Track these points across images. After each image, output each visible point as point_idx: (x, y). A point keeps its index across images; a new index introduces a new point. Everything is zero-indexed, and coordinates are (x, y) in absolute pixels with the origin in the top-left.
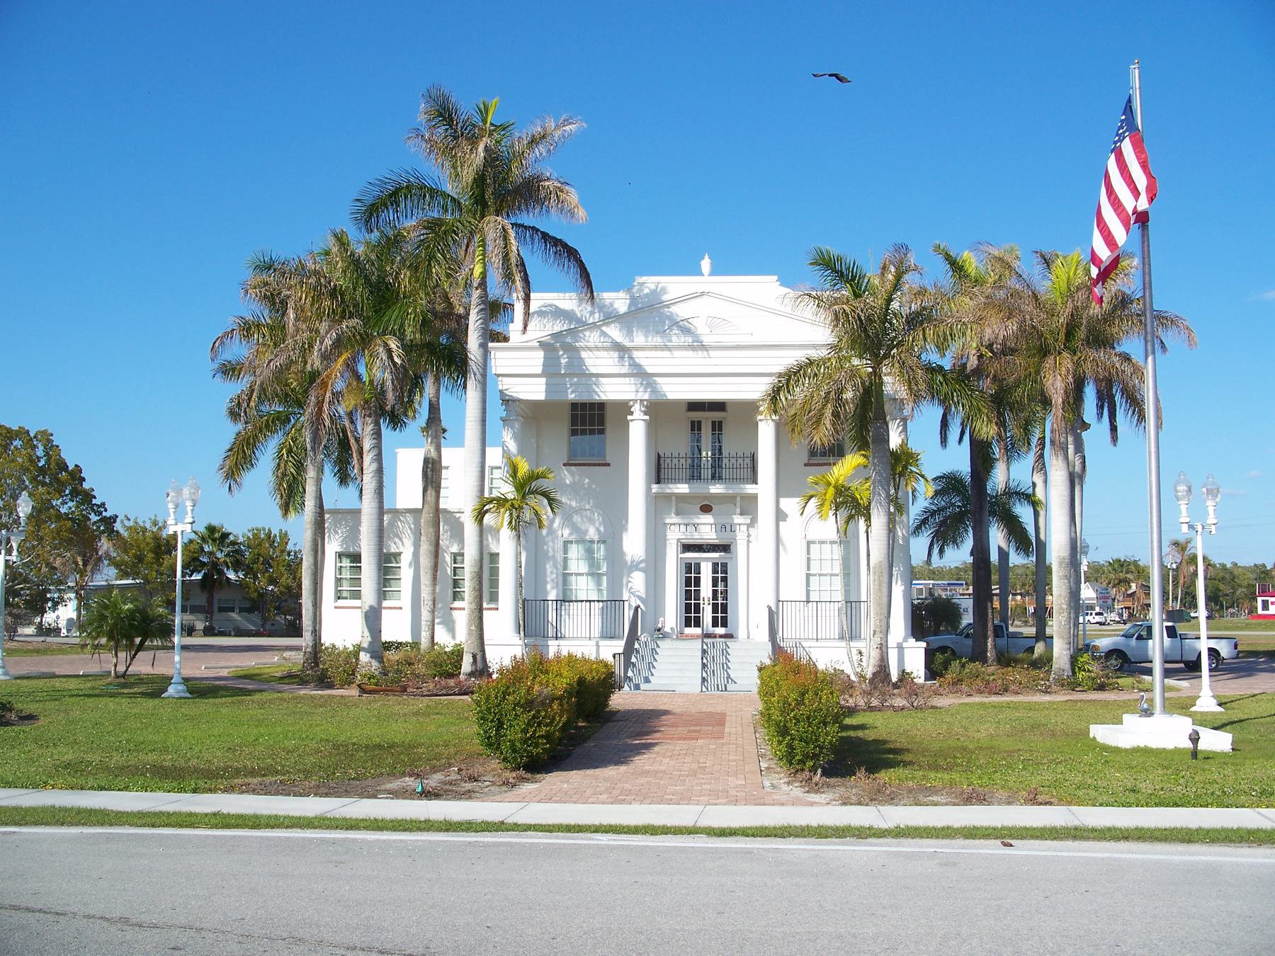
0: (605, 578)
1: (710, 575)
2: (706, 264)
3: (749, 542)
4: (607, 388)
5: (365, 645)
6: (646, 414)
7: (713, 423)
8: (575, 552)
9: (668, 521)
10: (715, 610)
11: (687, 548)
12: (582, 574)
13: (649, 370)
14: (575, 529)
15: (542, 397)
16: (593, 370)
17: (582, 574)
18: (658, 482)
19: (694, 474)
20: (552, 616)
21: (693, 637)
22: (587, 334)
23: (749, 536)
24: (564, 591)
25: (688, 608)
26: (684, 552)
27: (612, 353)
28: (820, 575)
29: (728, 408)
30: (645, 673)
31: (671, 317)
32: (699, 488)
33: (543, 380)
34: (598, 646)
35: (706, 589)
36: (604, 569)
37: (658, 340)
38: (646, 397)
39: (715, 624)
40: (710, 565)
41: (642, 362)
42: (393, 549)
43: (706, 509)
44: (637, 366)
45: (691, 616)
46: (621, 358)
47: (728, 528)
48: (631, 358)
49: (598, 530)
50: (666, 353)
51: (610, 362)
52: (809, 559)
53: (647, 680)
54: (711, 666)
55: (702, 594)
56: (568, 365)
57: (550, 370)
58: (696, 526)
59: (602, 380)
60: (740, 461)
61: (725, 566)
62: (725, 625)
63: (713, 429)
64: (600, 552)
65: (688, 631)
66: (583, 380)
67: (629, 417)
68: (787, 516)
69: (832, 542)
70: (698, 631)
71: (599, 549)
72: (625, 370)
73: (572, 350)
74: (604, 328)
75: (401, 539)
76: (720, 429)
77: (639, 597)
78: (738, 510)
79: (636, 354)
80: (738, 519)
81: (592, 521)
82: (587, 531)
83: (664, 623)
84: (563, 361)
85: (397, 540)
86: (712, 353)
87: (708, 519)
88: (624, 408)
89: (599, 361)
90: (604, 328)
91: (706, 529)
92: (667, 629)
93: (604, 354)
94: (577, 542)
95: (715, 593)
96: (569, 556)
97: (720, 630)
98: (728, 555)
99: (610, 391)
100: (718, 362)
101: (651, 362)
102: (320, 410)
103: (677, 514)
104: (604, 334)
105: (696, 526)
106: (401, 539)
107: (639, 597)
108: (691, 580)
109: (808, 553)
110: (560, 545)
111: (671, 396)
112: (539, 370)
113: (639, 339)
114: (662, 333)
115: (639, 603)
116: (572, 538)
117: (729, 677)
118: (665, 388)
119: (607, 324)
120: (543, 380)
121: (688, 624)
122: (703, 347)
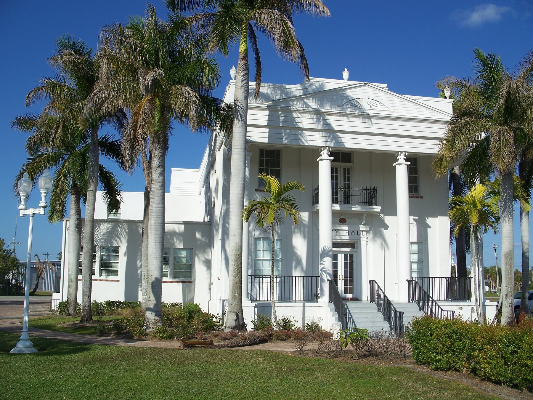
0: (280, 263)
1: (343, 262)
2: (346, 74)
4: (308, 138)
5: (152, 306)
6: (330, 156)
7: (345, 169)
12: (266, 260)
13: (336, 128)
15: (266, 141)
16: (301, 126)
17: (266, 260)
22: (295, 102)
27: (312, 115)
29: (355, 158)
31: (347, 97)
33: (267, 130)
34: (304, 306)
36: (280, 257)
37: (339, 110)
38: (332, 145)
41: (332, 123)
42: (115, 244)
44: (329, 125)
46: (318, 119)
48: (324, 119)
50: (345, 119)
51: (311, 121)
56: (284, 121)
57: (272, 125)
59: (307, 133)
60: (360, 191)
61: (352, 256)
63: (345, 173)
64: (278, 246)
66: (293, 132)
68: (388, 227)
72: (320, 127)
73: (288, 111)
74: (305, 100)
75: (120, 238)
76: (348, 173)
77: (329, 274)
79: (328, 117)
80: (362, 228)
84: (282, 118)
85: (117, 239)
86: (373, 121)
87: (345, 227)
88: (316, 151)
89: (305, 121)
90: (305, 100)
93: (308, 116)
94: (263, 240)
95: (346, 272)
96: (258, 248)
98: (354, 250)
99: (314, 139)
100: (378, 126)
101: (337, 123)
102: (135, 132)
104: (305, 103)
106: (120, 238)
111: (347, 146)
112: (265, 123)
113: (327, 109)
114: (342, 106)
118: (344, 140)
119: (308, 98)
120: (267, 130)
122: (368, 117)
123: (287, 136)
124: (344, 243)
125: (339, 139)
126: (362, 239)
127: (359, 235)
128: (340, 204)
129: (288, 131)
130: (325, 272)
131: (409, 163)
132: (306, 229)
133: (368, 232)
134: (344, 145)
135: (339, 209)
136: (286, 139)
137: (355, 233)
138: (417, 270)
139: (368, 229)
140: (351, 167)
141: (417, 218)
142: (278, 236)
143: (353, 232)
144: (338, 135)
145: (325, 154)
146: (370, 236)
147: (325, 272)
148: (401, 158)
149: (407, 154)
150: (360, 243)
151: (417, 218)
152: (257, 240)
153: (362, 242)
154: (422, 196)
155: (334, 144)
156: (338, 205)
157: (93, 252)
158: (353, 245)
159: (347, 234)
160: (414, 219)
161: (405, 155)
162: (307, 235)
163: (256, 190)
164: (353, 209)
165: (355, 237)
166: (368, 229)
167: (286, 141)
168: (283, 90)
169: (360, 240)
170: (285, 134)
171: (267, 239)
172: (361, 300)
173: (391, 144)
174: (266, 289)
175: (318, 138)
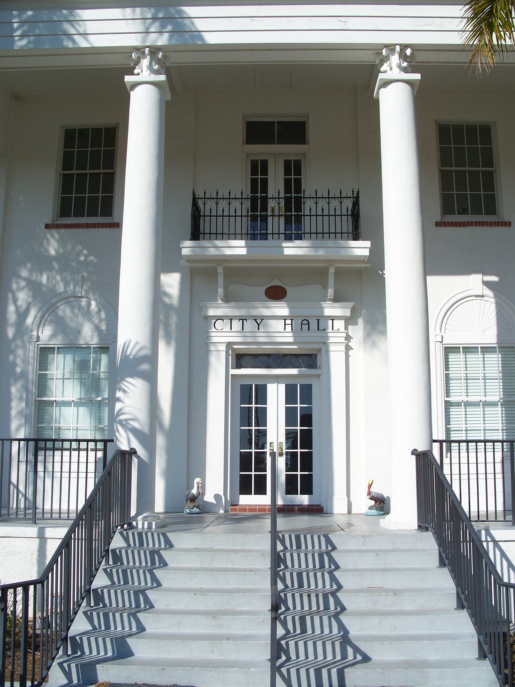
1: (283, 406)
3: (348, 348)
7: (287, 164)
8: (60, 366)
9: (212, 312)
10: (291, 466)
11: (240, 359)
14: (61, 326)
18: (195, 236)
19: (256, 229)
20: (18, 474)
21: (255, 513)
23: (348, 338)
24: (39, 430)
25: (245, 462)
26: (239, 366)
28: (467, 404)
30: (120, 625)
32: (264, 249)
35: (276, 431)
38: (163, 40)
39: (291, 489)
40: (282, 388)
43: (276, 294)
45: (249, 472)
47: (313, 324)
49: (97, 328)
52: (447, 377)
53: (122, 652)
54: (296, 604)
55: (271, 437)
58: (259, 321)
62: (307, 489)
63: (287, 172)
65: (245, 500)
67: (128, 79)
69: (486, 350)
70: (265, 500)
71: (98, 361)
76: (298, 172)
77: (135, 432)
78: (331, 292)
80: (330, 310)
81: (87, 313)
82: (78, 332)
83: (202, 486)
87: (281, 309)
91: (278, 327)
92: (209, 498)
95: (290, 436)
97: (304, 499)
103: (227, 299)
105: (259, 321)
107: (135, 432)
108: (249, 401)
109: (447, 368)
110: (32, 352)
111: (211, 39)
115: (136, 445)
116: (57, 342)
117: (346, 640)
118: (200, 25)
121: (245, 489)
123: (26, 28)
124: (285, 355)
125: (186, 21)
126: (331, 340)
127: (321, 329)
128: (246, 239)
129: (30, 13)
130: (124, 424)
131: (417, 76)
132: (174, 320)
133: (349, 321)
134: (201, 38)
135: (243, 252)
136: (22, 36)
137: (310, 324)
138: (500, 426)
139: (348, 313)
140: (304, 155)
141: (494, 279)
142: (100, 339)
143: (306, 322)
144: (182, 12)
145: (144, 71)
146: (357, 331)
147: (124, 424)
148: (392, 68)
149: (408, 52)
150: (327, 352)
151: (494, 279)
152: (45, 353)
153: (332, 348)
154: (506, 219)
155: (170, 38)
156: (242, 243)
157: (39, 423)
158: (310, 359)
159: (289, 328)
160: (485, 283)
161: (403, 56)
162: (174, 335)
163: (47, 226)
164: (288, 252)
165: (311, 336)
166: (348, 313)
167: (24, 42)
168: (179, 27)
169: (326, 344)
170: (22, 23)
171: (71, 347)
172: (330, 513)
173: (352, 24)
174: (74, 481)
175: (123, 26)
